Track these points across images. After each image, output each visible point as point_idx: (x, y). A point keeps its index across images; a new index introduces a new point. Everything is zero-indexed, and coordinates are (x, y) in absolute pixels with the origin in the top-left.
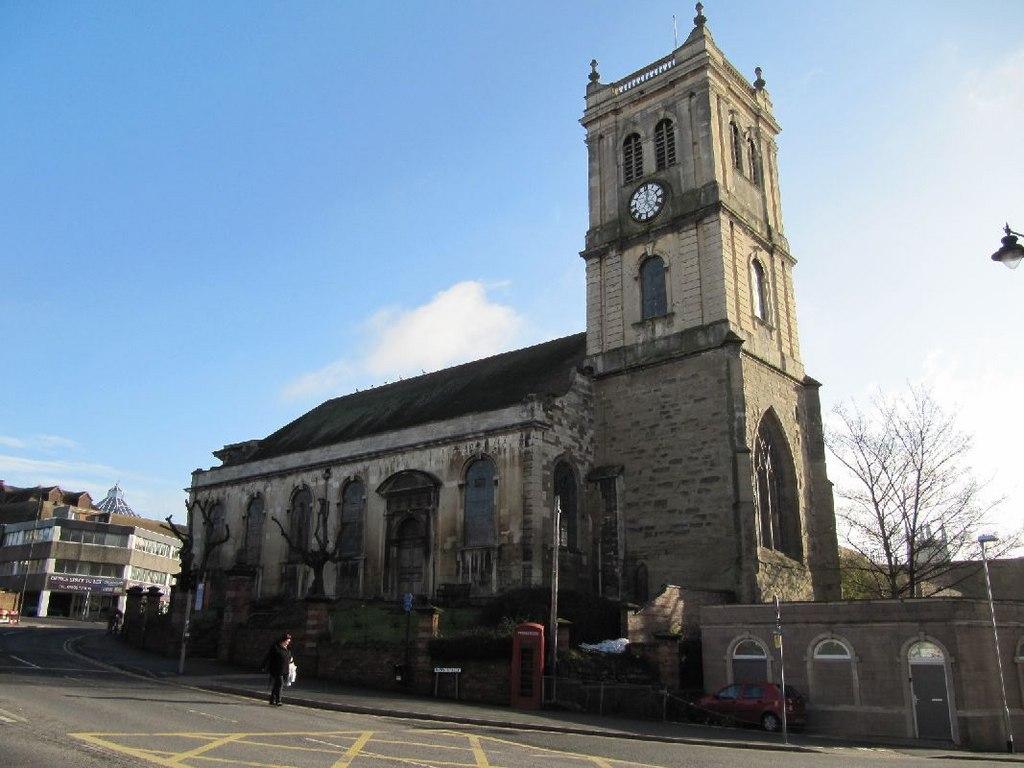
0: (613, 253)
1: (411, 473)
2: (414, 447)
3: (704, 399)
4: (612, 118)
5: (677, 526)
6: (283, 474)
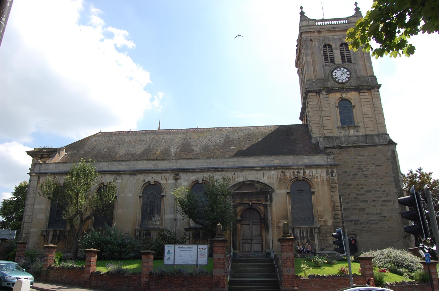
1: (252, 184)
2: (252, 168)
4: (316, 34)
5: (371, 220)
6: (133, 173)
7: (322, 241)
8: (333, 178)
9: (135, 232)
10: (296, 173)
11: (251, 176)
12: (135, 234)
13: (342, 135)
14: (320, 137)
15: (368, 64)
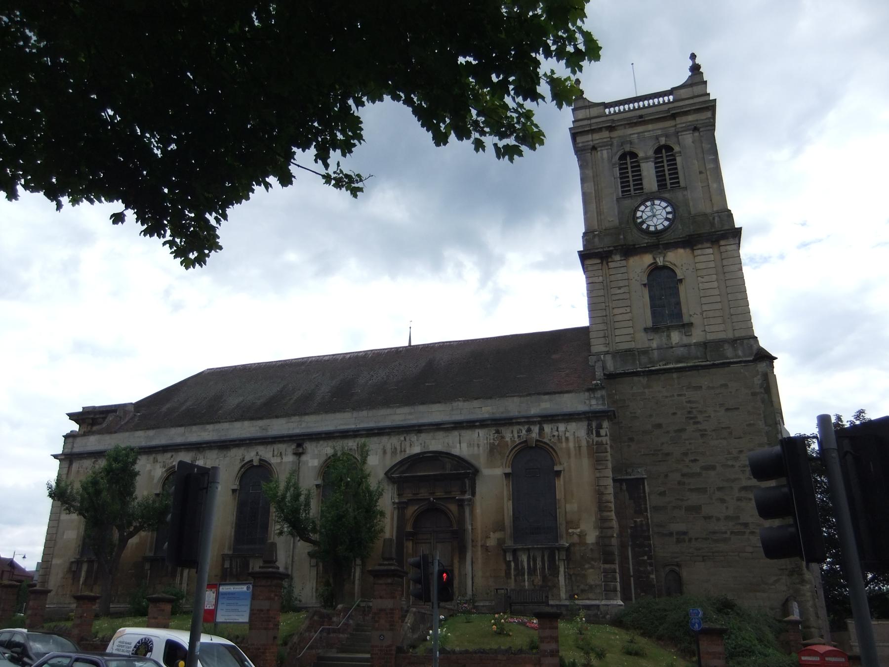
2: (438, 427)
4: (606, 134)
5: (714, 533)
6: (224, 445)
7: (573, 579)
8: (599, 439)
9: (223, 560)
10: (524, 432)
11: (436, 443)
12: (223, 565)
13: (654, 345)
14: (607, 353)
15: (715, 186)
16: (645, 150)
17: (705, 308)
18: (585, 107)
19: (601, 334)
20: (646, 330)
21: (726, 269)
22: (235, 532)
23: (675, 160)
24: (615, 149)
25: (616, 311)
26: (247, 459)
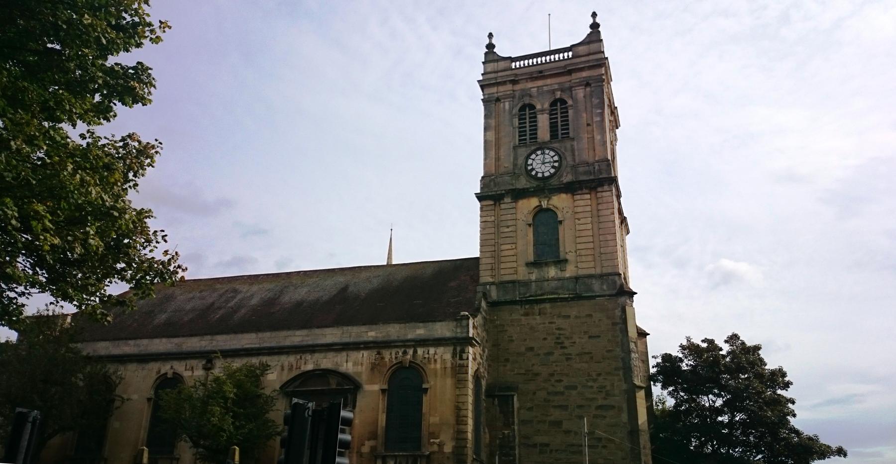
0: (507, 200)
1: (327, 373)
3: (599, 337)
4: (509, 87)
5: (573, 445)
6: (143, 359)
8: (462, 362)
11: (327, 361)
13: (533, 277)
16: (542, 104)
17: (579, 247)
18: (497, 61)
19: (489, 267)
20: (528, 265)
21: (601, 213)
22: (148, 436)
23: (567, 112)
24: (516, 100)
25: (503, 247)
26: (163, 372)
